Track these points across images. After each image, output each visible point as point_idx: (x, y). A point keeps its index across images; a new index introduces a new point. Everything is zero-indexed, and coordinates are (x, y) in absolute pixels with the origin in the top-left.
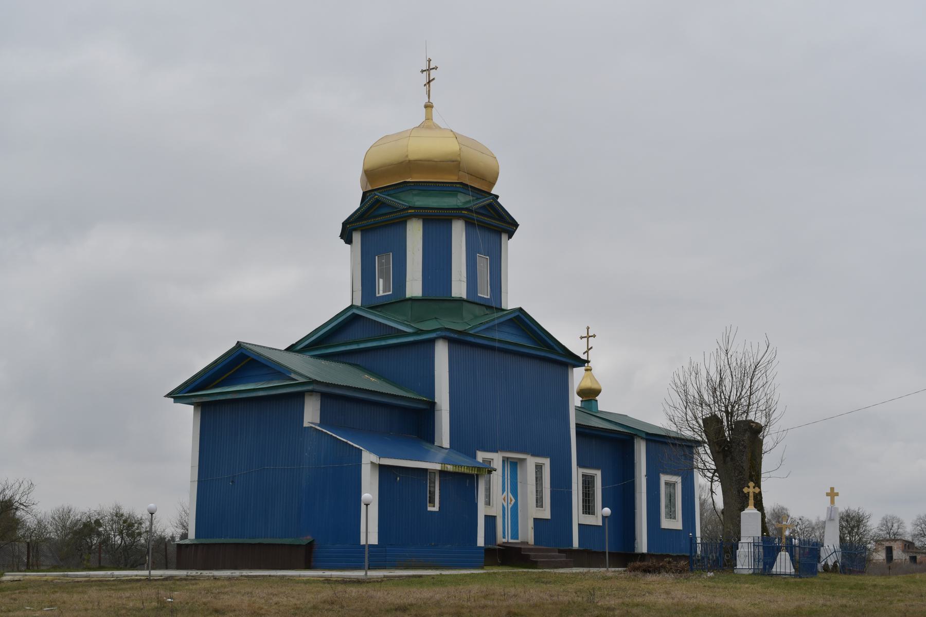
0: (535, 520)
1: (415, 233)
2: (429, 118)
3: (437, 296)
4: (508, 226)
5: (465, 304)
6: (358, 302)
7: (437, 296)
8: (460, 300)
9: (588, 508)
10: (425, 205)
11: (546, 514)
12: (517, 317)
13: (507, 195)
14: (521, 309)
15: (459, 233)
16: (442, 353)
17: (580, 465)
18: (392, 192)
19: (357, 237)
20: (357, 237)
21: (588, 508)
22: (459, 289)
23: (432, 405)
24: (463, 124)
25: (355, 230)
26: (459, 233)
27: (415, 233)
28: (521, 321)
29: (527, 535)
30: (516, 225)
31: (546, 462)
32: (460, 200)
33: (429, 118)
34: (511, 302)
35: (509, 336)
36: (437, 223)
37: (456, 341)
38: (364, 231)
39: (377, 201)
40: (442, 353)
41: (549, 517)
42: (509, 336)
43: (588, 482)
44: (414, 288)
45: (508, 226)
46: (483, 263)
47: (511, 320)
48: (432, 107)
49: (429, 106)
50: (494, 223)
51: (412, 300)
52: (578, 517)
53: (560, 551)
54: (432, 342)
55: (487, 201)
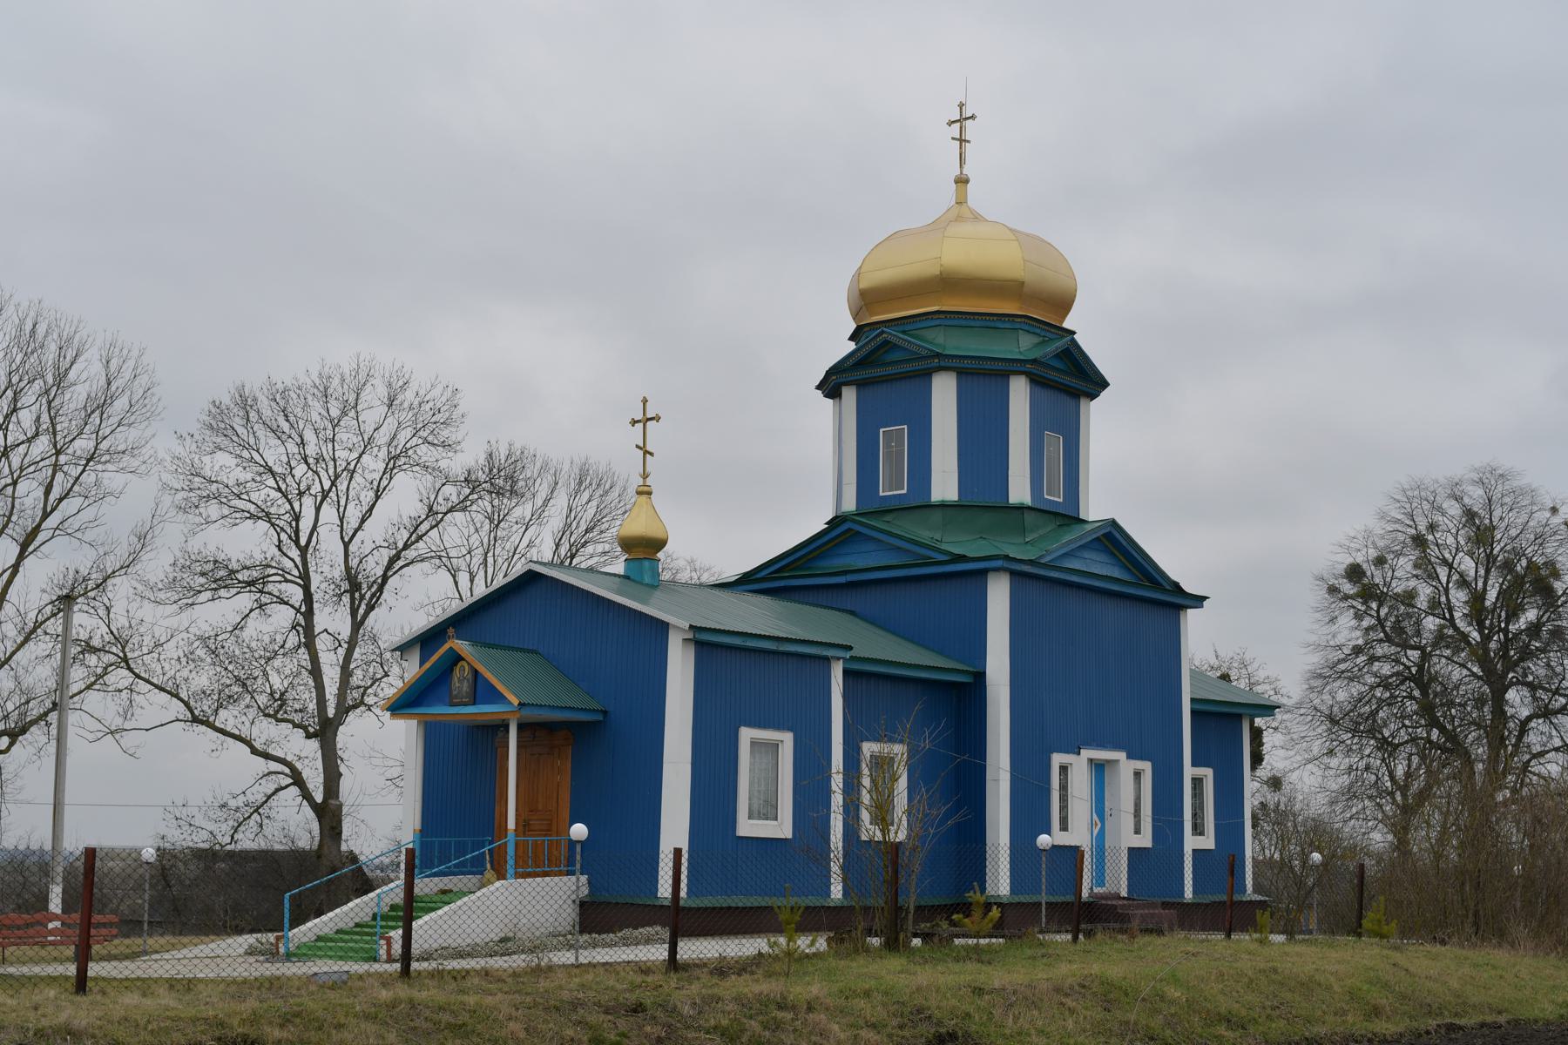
0: (1131, 850)
1: (944, 393)
2: (961, 201)
3: (983, 502)
4: (1093, 383)
5: (1029, 518)
6: (850, 505)
7: (983, 502)
8: (1021, 508)
9: (1198, 830)
10: (964, 353)
11: (1145, 840)
12: (1108, 536)
13: (1088, 327)
14: (1113, 523)
15: (1019, 392)
16: (999, 596)
17: (1194, 764)
18: (907, 328)
19: (850, 394)
20: (850, 394)
21: (1198, 830)
22: (1019, 491)
23: (980, 677)
24: (1017, 209)
25: (847, 384)
26: (1019, 392)
27: (944, 393)
28: (1113, 539)
29: (1118, 882)
30: (1103, 384)
31: (1146, 766)
32: (1024, 346)
33: (961, 201)
34: (1095, 508)
35: (1100, 566)
36: (983, 380)
37: (1021, 577)
38: (861, 385)
39: (886, 342)
40: (999, 596)
41: (1149, 845)
42: (1100, 566)
43: (1197, 782)
44: (945, 485)
45: (1093, 383)
46: (1054, 444)
47: (1098, 539)
48: (967, 181)
49: (962, 181)
50: (1071, 379)
51: (943, 506)
52: (1191, 843)
53: (1165, 905)
54: (983, 574)
55: (1060, 344)
